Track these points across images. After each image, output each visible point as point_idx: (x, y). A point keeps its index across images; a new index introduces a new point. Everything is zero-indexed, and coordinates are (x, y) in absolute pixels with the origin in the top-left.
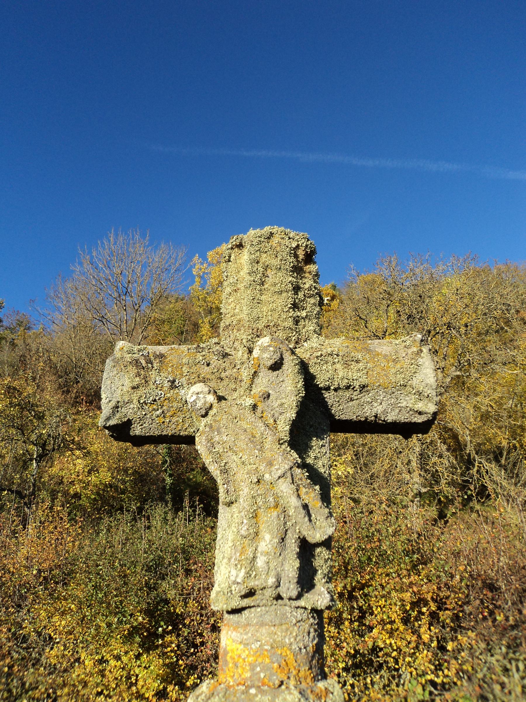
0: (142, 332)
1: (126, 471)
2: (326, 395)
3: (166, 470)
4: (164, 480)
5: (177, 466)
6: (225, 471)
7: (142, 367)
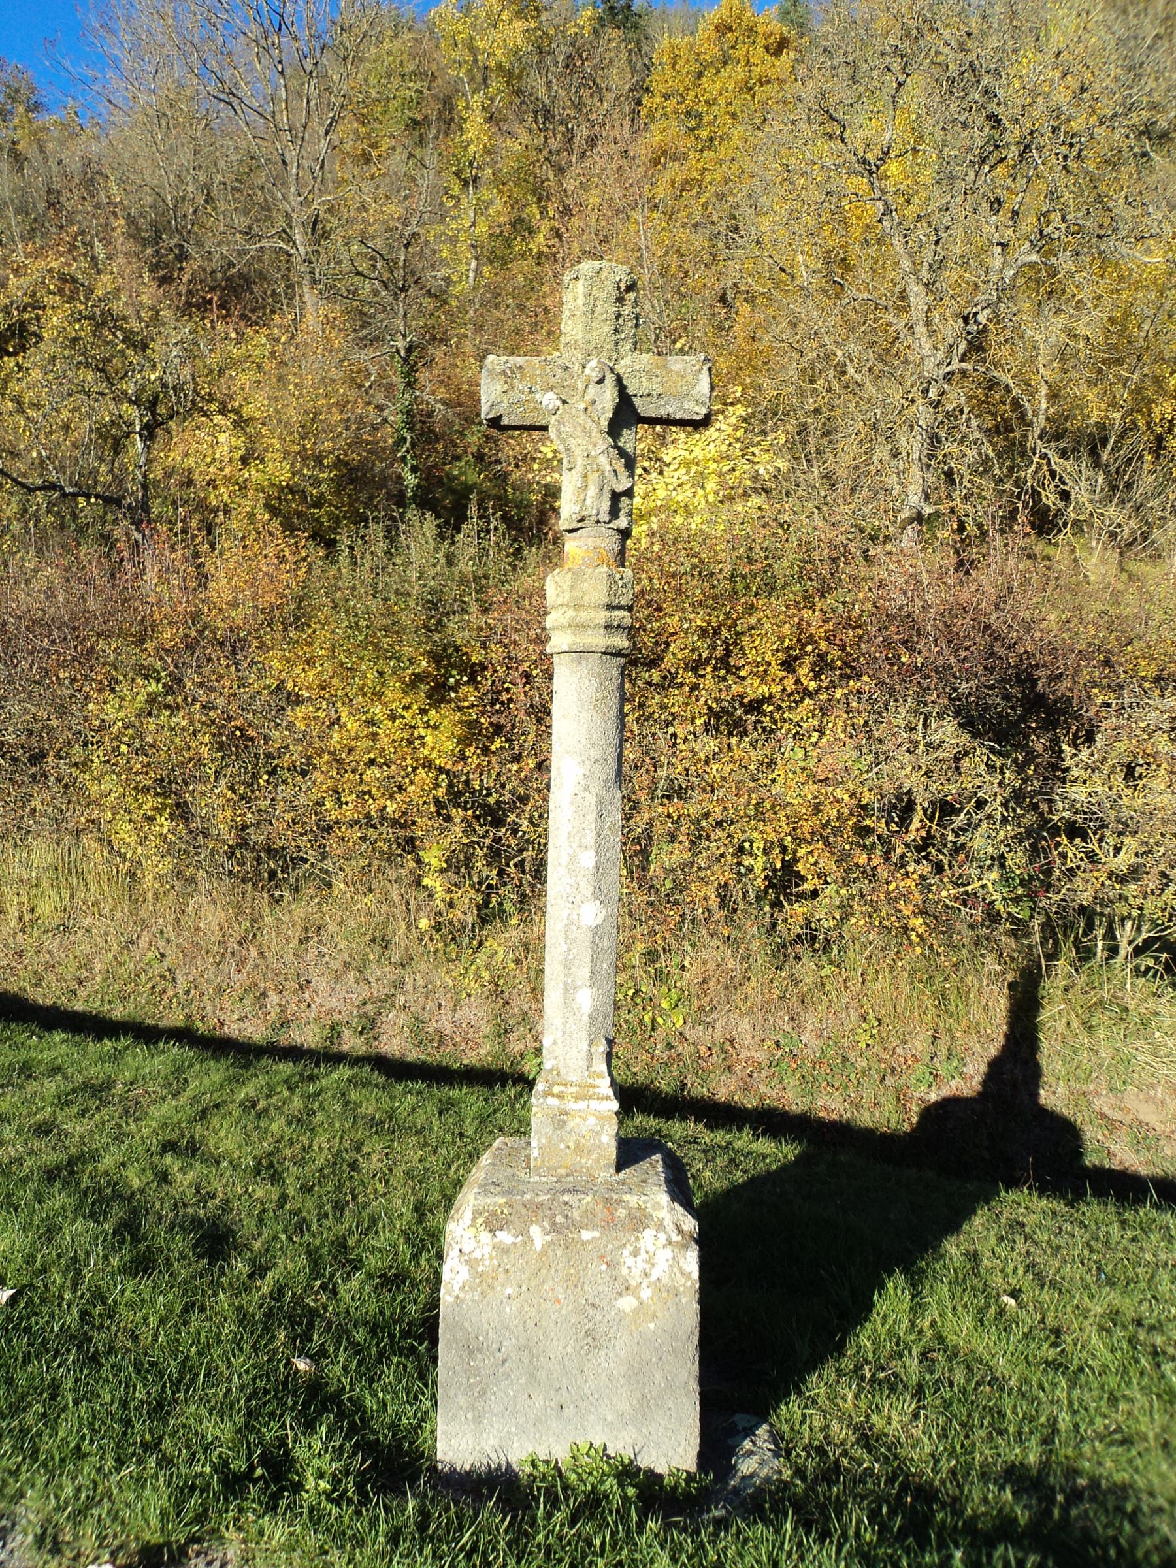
0: (327, 133)
1: (319, 459)
3: (403, 459)
4: (400, 477)
5: (423, 450)
7: (508, 375)
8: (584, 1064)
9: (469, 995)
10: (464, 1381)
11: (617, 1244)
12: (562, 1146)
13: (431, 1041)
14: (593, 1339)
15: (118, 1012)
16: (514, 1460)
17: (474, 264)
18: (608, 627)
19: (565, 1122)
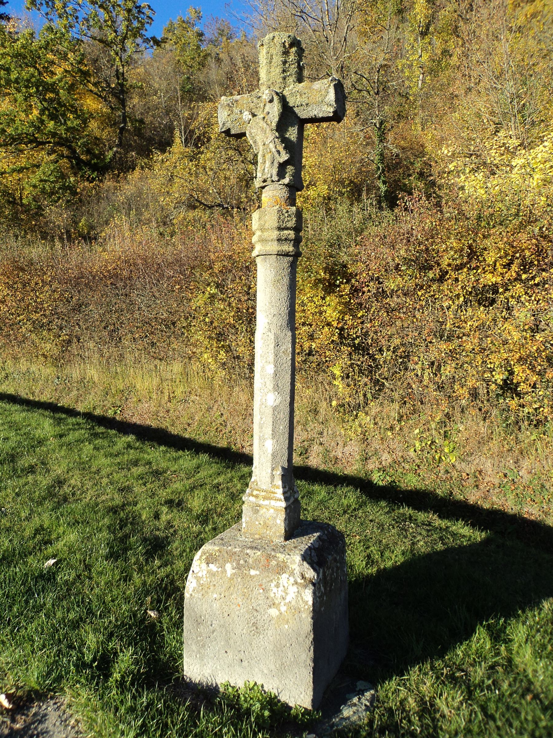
2: (295, 109)
6: (255, 142)
8: (269, 480)
9: (351, 440)
10: (195, 638)
11: (268, 579)
12: (257, 523)
13: (331, 461)
14: (256, 628)
15: (202, 439)
16: (219, 683)
17: (421, 76)
18: (279, 240)
19: (258, 511)
